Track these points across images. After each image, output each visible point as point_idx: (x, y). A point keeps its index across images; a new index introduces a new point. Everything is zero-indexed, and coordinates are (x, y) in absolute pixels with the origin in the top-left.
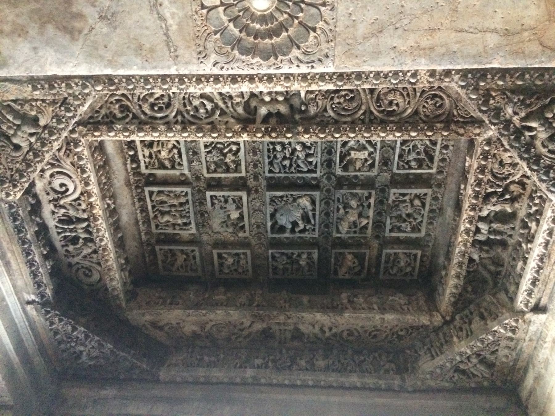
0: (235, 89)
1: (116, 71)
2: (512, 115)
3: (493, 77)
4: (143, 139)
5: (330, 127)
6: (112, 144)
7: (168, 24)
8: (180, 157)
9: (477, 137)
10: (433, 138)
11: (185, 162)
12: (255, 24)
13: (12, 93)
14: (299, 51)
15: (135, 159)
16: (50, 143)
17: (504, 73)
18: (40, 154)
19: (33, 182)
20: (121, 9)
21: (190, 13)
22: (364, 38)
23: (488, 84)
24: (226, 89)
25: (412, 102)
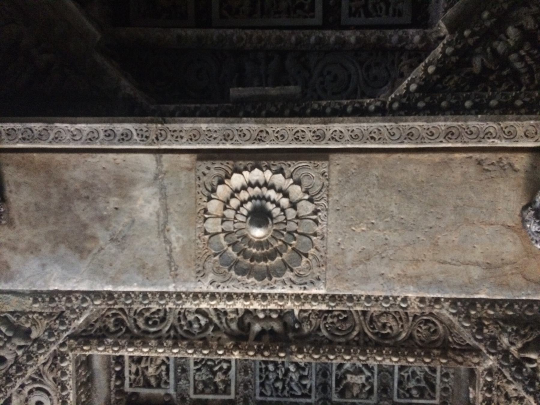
0: (230, 305)
1: (115, 287)
2: (509, 345)
3: (483, 305)
4: (132, 354)
5: (324, 347)
6: (100, 359)
7: (173, 246)
8: (168, 374)
9: (477, 367)
10: (432, 365)
11: (172, 381)
12: (252, 249)
13: (13, 304)
14: (292, 274)
15: (120, 376)
16: (37, 357)
17: (493, 303)
18: (24, 368)
19: (10, 398)
20: (131, 233)
21: (194, 238)
22: (353, 265)
23: (479, 312)
24: (221, 306)
25: (406, 326)
